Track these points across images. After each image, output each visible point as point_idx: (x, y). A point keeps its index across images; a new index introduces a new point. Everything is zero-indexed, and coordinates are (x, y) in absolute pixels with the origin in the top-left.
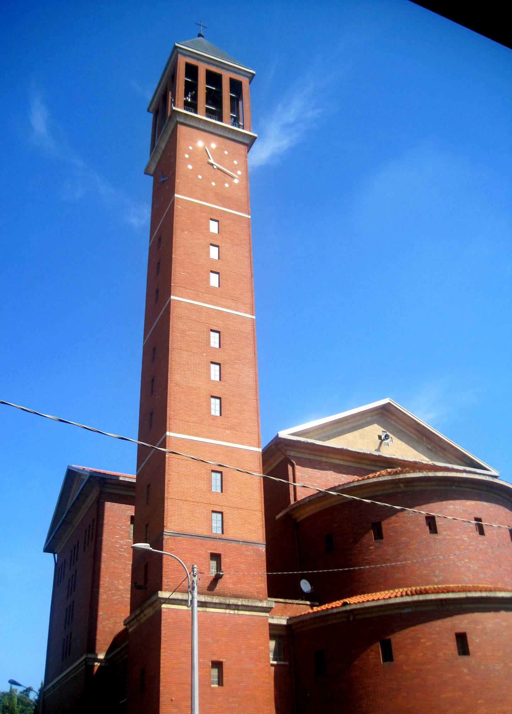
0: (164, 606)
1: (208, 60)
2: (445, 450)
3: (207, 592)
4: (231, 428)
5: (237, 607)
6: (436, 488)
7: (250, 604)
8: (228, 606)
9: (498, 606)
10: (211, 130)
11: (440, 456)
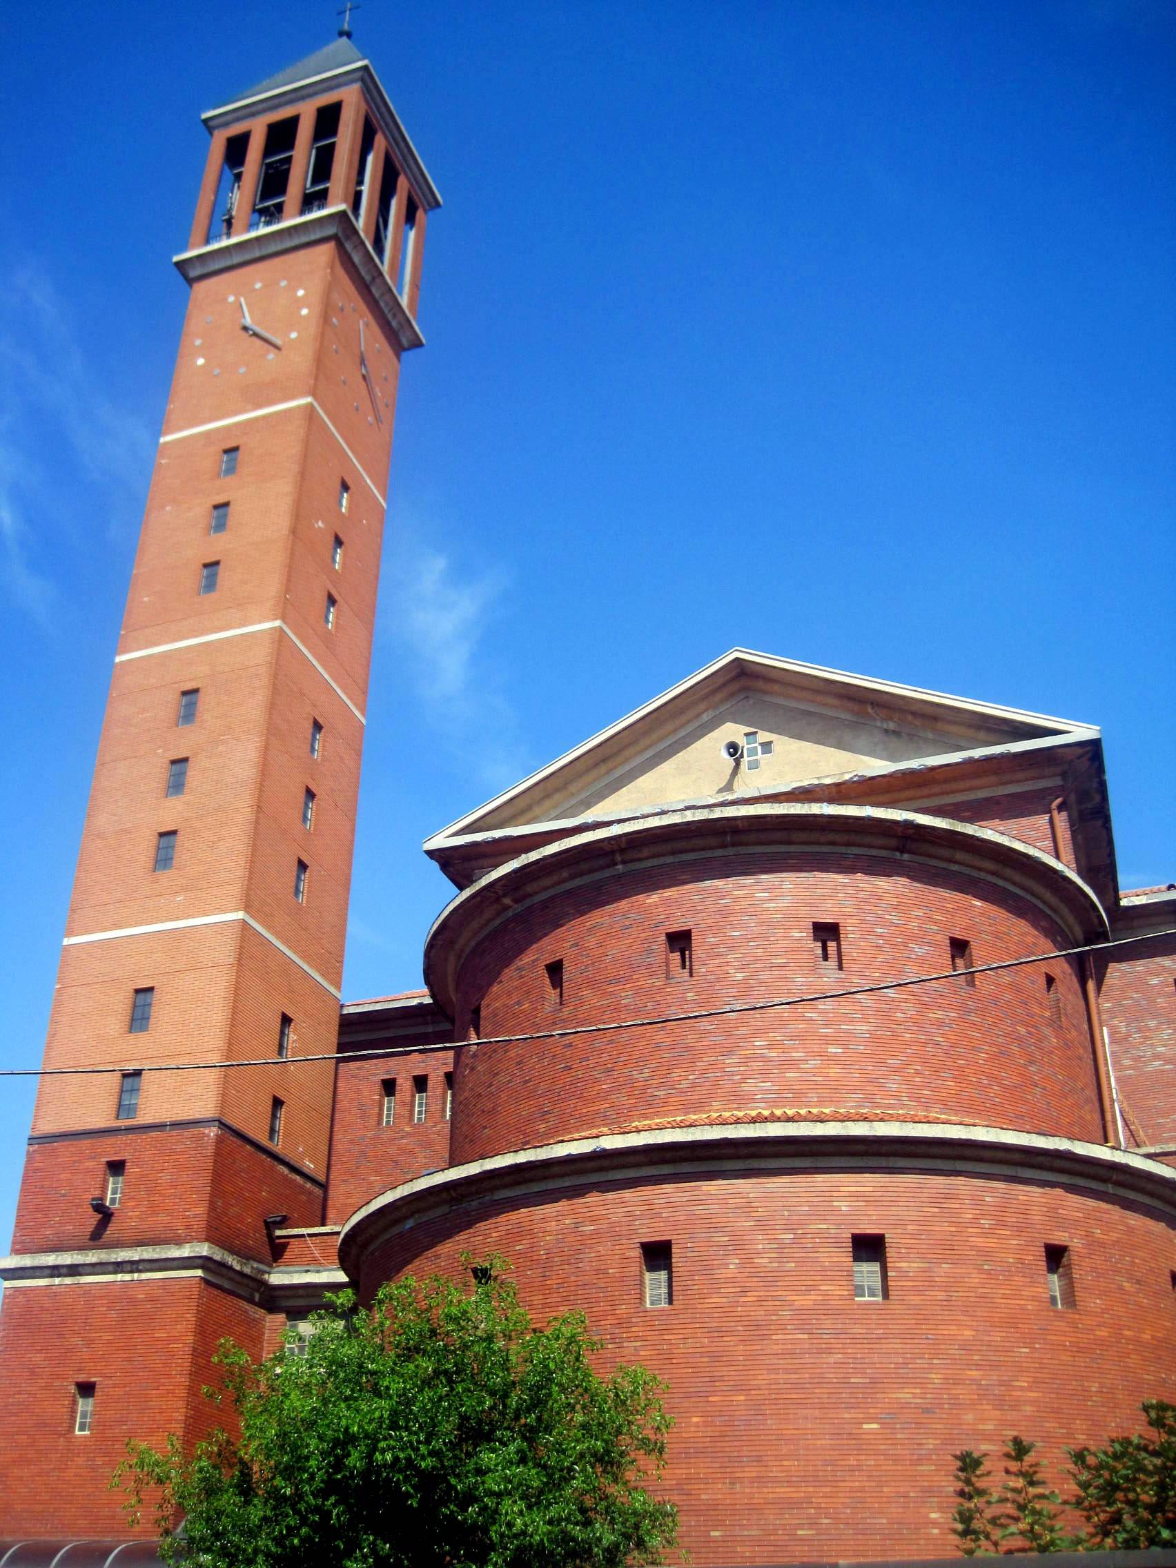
1: (270, 103)
3: (92, 1243)
4: (185, 889)
5: (134, 1266)
7: (156, 1256)
8: (119, 1267)
10: (257, 254)
11: (926, 740)
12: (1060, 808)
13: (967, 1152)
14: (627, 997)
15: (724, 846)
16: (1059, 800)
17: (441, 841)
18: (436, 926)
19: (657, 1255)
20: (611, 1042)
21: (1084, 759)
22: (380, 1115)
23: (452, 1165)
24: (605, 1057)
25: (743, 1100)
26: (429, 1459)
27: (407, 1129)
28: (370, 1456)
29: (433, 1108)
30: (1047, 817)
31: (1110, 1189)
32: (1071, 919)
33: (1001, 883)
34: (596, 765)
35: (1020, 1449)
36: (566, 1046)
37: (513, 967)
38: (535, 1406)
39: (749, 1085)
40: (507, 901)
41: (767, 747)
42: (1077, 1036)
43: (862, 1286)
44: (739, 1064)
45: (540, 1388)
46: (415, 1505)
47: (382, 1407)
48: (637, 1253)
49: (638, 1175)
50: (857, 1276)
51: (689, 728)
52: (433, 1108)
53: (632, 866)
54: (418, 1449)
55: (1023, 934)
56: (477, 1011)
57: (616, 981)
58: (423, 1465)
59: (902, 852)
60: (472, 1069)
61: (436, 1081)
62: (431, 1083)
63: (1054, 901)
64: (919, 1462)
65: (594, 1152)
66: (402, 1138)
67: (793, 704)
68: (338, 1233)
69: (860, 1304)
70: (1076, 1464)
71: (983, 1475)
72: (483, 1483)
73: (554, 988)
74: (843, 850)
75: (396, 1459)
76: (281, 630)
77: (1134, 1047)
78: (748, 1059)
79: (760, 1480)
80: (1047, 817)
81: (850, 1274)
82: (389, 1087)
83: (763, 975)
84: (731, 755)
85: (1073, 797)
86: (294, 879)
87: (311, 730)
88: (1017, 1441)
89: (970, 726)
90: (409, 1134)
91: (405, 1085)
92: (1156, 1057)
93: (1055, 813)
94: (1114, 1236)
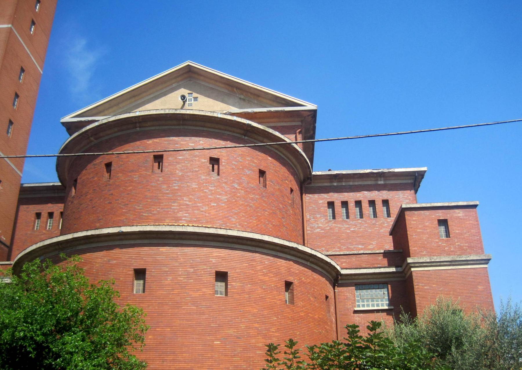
0: (412, 269)
2: (258, 96)
6: (119, 134)
9: (110, 244)
11: (254, 103)
12: (300, 133)
13: (261, 244)
14: (136, 177)
15: (179, 125)
16: (299, 130)
17: (68, 119)
18: (63, 147)
19: (140, 274)
20: (128, 194)
21: (309, 117)
22: (34, 226)
23: (62, 234)
24: (125, 199)
25: (177, 219)
26: (41, 337)
27: (44, 232)
28: (13, 335)
29: (54, 225)
30: (294, 136)
31: (309, 264)
32: (300, 171)
33: (279, 153)
34: (131, 98)
35: (292, 344)
36: (110, 195)
37: (92, 164)
38: (91, 317)
39: (180, 214)
40: (92, 139)
41: (196, 99)
42: (299, 211)
43: (218, 291)
44: (177, 206)
45: (93, 309)
46: (33, 357)
47: (20, 314)
48: (132, 273)
49: (135, 243)
50: (216, 287)
51: (168, 89)
52: (54, 225)
53: (143, 129)
54: (36, 332)
55: (285, 172)
56: (76, 181)
57: (132, 171)
58: (38, 339)
59: (245, 136)
60: (72, 202)
61: (57, 214)
62: (55, 215)
63: (296, 163)
64: (234, 356)
65: (119, 232)
66: (42, 235)
67: (207, 85)
68: (11, 264)
69: (216, 297)
70: (310, 351)
71: (277, 353)
72: (65, 348)
73: (108, 172)
74: (223, 132)
75: (25, 336)
76: (11, 28)
77: (311, 223)
78: (180, 205)
79: (174, 360)
80: (294, 136)
81: (214, 286)
82: (38, 215)
83: (189, 174)
84: (182, 99)
85: (303, 131)
86: (7, 127)
87: (20, 71)
88: (291, 341)
89: (270, 100)
90: (44, 234)
91: (44, 215)
92: (318, 228)
93: (298, 134)
94: (309, 280)
